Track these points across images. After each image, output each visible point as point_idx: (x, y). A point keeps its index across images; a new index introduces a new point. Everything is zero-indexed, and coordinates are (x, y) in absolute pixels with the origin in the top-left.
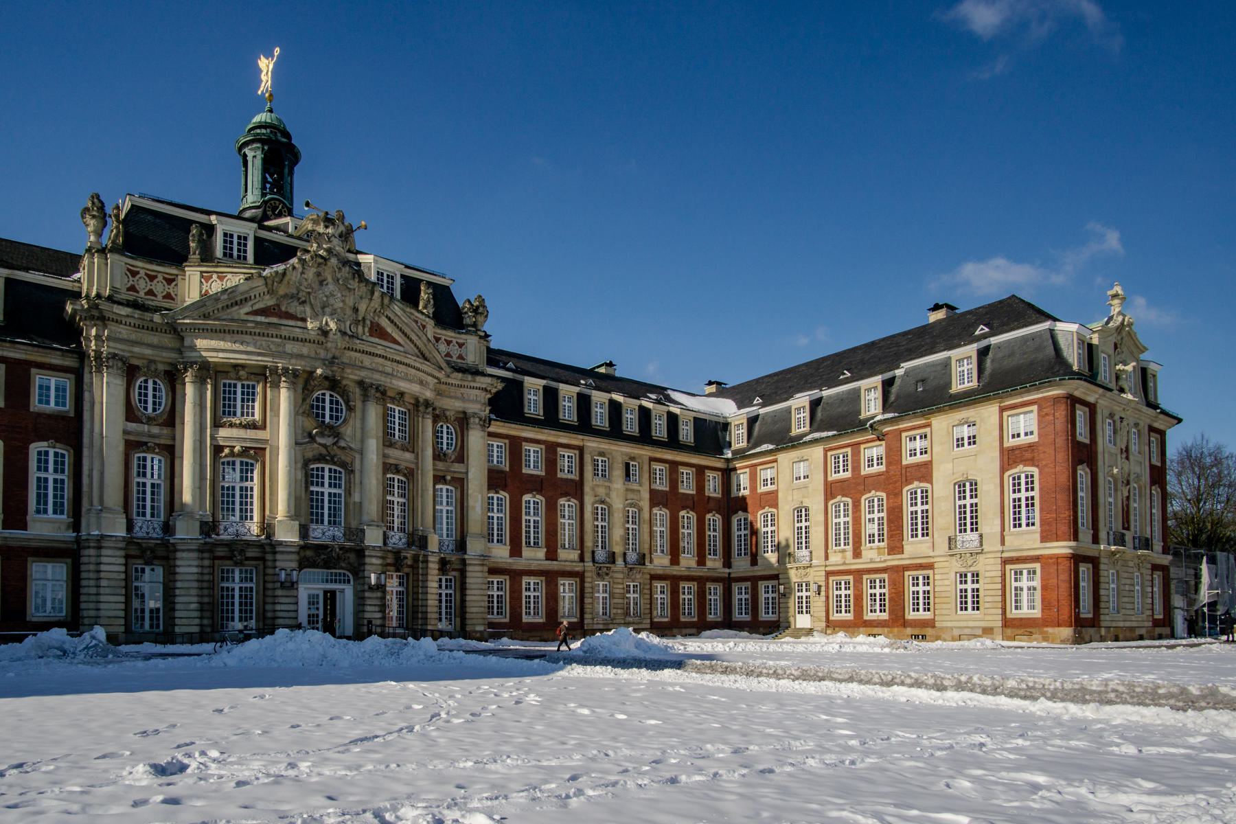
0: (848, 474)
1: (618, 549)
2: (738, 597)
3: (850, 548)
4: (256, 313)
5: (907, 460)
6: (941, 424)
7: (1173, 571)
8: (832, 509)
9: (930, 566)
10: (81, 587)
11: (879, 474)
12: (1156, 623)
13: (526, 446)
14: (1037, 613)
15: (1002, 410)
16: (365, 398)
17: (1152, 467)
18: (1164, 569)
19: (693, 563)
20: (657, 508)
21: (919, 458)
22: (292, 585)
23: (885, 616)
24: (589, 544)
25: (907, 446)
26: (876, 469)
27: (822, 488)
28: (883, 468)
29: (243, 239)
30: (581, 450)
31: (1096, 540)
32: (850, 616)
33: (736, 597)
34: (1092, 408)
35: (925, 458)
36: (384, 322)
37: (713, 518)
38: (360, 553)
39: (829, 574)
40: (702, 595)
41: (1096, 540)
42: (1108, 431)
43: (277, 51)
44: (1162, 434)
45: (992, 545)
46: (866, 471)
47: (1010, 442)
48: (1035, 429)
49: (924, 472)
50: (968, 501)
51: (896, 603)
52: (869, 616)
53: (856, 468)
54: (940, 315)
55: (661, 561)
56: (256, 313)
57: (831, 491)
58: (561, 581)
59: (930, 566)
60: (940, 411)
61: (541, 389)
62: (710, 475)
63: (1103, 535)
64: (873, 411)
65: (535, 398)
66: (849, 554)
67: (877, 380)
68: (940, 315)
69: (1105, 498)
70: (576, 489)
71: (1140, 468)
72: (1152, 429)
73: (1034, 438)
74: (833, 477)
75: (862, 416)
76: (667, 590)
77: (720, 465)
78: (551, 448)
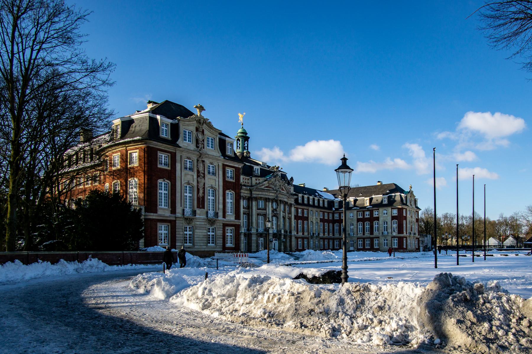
0: (362, 217)
1: (314, 232)
2: (336, 243)
3: (362, 233)
4: (265, 187)
5: (375, 216)
6: (381, 210)
7: (420, 239)
8: (358, 224)
9: (379, 238)
10: (446, 251)
11: (368, 218)
12: (417, 249)
13: (159, 154)
14: (397, 247)
15: (392, 209)
16: (280, 203)
17: (416, 219)
18: (418, 239)
19: (327, 235)
20: (229, 191)
21: (377, 216)
22: (272, 241)
23: (369, 247)
24: (309, 231)
25: (374, 213)
26: (368, 216)
27: (356, 219)
28: (369, 217)
29: (258, 169)
30: (308, 210)
31: (406, 234)
32: (362, 247)
33: (335, 243)
34: (406, 209)
35: (378, 216)
36: (283, 188)
37: (331, 225)
38: (280, 235)
39: (358, 238)
40: (329, 243)
41: (406, 234)
42: (409, 213)
43: (244, 114)
44: (418, 212)
45: (390, 234)
46: (366, 217)
47: (393, 215)
48: (397, 213)
49: (377, 219)
50: (386, 225)
51: (372, 244)
52: (366, 247)
53: (364, 216)
54: (379, 184)
55: (321, 235)
56: (265, 187)
57: (359, 220)
58: (159, 225)
59: (379, 238)
60: (381, 207)
61: (169, 124)
62: (330, 214)
63: (408, 233)
64: (367, 205)
65: (166, 129)
66: (362, 234)
67: (368, 198)
68: (379, 184)
69: (408, 226)
70: (307, 219)
71: (414, 220)
72: (416, 211)
73: (397, 215)
74: (359, 217)
75: (365, 205)
76: (302, 241)
77: (332, 212)
78: (303, 209)
